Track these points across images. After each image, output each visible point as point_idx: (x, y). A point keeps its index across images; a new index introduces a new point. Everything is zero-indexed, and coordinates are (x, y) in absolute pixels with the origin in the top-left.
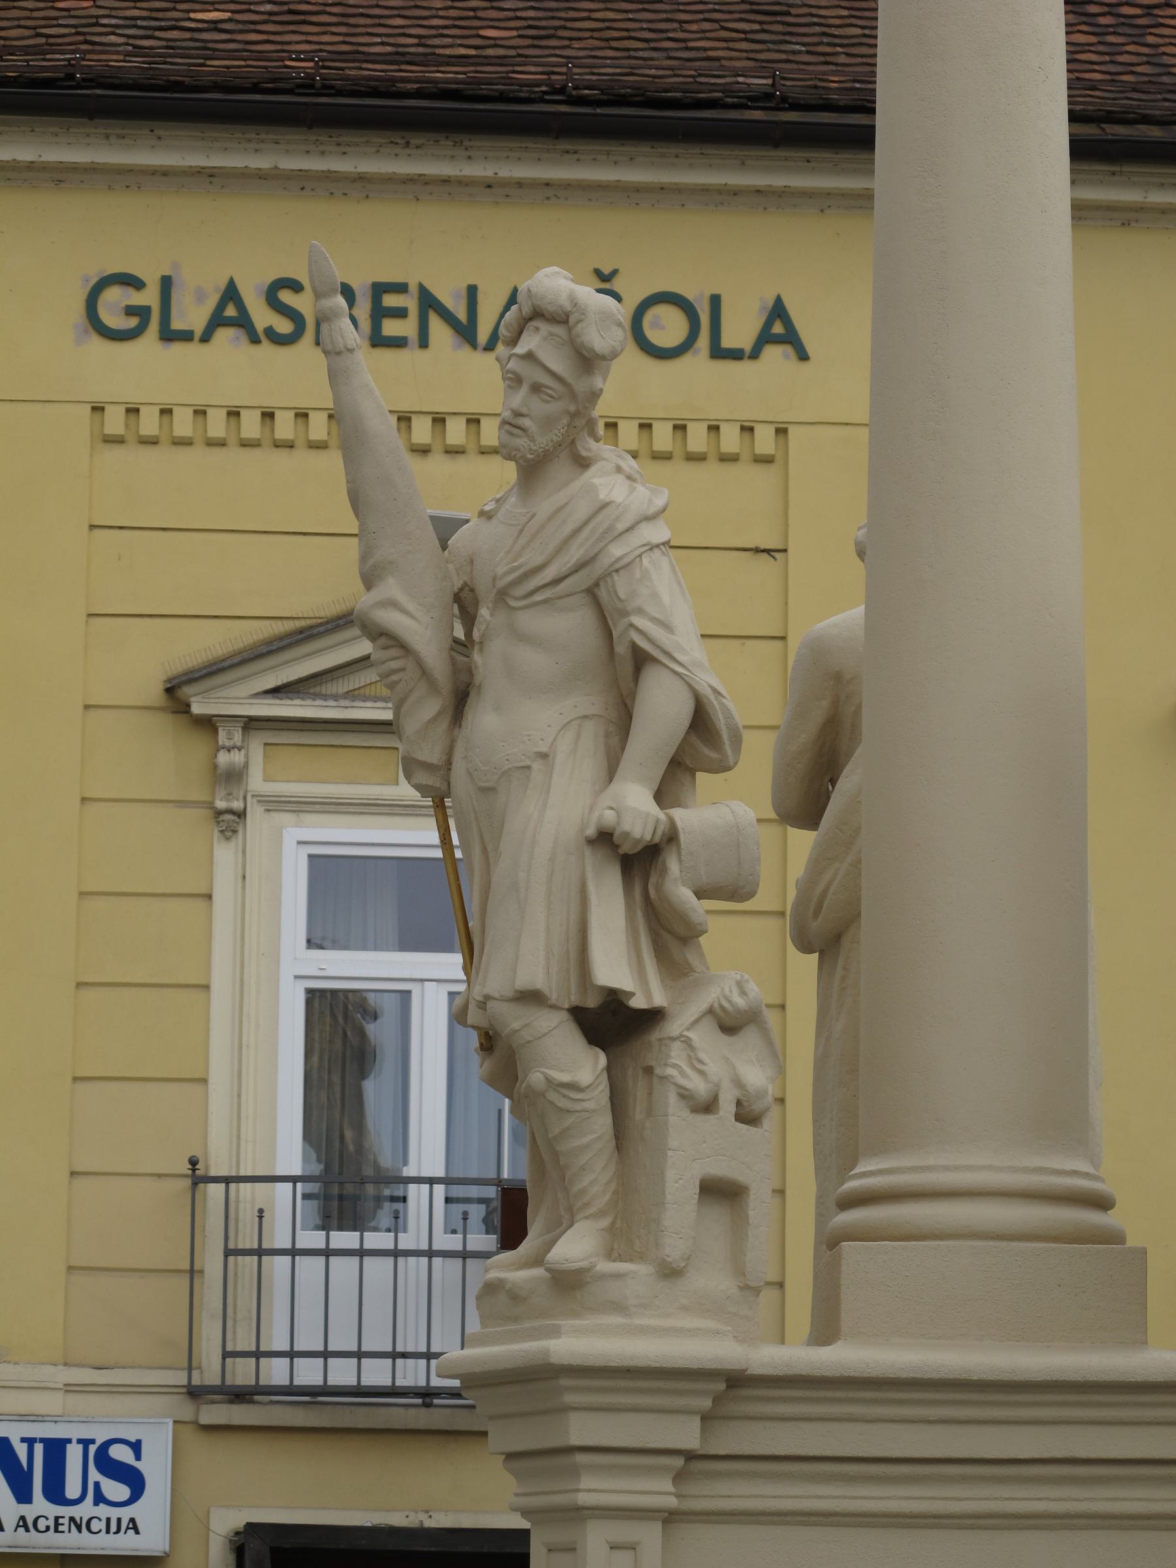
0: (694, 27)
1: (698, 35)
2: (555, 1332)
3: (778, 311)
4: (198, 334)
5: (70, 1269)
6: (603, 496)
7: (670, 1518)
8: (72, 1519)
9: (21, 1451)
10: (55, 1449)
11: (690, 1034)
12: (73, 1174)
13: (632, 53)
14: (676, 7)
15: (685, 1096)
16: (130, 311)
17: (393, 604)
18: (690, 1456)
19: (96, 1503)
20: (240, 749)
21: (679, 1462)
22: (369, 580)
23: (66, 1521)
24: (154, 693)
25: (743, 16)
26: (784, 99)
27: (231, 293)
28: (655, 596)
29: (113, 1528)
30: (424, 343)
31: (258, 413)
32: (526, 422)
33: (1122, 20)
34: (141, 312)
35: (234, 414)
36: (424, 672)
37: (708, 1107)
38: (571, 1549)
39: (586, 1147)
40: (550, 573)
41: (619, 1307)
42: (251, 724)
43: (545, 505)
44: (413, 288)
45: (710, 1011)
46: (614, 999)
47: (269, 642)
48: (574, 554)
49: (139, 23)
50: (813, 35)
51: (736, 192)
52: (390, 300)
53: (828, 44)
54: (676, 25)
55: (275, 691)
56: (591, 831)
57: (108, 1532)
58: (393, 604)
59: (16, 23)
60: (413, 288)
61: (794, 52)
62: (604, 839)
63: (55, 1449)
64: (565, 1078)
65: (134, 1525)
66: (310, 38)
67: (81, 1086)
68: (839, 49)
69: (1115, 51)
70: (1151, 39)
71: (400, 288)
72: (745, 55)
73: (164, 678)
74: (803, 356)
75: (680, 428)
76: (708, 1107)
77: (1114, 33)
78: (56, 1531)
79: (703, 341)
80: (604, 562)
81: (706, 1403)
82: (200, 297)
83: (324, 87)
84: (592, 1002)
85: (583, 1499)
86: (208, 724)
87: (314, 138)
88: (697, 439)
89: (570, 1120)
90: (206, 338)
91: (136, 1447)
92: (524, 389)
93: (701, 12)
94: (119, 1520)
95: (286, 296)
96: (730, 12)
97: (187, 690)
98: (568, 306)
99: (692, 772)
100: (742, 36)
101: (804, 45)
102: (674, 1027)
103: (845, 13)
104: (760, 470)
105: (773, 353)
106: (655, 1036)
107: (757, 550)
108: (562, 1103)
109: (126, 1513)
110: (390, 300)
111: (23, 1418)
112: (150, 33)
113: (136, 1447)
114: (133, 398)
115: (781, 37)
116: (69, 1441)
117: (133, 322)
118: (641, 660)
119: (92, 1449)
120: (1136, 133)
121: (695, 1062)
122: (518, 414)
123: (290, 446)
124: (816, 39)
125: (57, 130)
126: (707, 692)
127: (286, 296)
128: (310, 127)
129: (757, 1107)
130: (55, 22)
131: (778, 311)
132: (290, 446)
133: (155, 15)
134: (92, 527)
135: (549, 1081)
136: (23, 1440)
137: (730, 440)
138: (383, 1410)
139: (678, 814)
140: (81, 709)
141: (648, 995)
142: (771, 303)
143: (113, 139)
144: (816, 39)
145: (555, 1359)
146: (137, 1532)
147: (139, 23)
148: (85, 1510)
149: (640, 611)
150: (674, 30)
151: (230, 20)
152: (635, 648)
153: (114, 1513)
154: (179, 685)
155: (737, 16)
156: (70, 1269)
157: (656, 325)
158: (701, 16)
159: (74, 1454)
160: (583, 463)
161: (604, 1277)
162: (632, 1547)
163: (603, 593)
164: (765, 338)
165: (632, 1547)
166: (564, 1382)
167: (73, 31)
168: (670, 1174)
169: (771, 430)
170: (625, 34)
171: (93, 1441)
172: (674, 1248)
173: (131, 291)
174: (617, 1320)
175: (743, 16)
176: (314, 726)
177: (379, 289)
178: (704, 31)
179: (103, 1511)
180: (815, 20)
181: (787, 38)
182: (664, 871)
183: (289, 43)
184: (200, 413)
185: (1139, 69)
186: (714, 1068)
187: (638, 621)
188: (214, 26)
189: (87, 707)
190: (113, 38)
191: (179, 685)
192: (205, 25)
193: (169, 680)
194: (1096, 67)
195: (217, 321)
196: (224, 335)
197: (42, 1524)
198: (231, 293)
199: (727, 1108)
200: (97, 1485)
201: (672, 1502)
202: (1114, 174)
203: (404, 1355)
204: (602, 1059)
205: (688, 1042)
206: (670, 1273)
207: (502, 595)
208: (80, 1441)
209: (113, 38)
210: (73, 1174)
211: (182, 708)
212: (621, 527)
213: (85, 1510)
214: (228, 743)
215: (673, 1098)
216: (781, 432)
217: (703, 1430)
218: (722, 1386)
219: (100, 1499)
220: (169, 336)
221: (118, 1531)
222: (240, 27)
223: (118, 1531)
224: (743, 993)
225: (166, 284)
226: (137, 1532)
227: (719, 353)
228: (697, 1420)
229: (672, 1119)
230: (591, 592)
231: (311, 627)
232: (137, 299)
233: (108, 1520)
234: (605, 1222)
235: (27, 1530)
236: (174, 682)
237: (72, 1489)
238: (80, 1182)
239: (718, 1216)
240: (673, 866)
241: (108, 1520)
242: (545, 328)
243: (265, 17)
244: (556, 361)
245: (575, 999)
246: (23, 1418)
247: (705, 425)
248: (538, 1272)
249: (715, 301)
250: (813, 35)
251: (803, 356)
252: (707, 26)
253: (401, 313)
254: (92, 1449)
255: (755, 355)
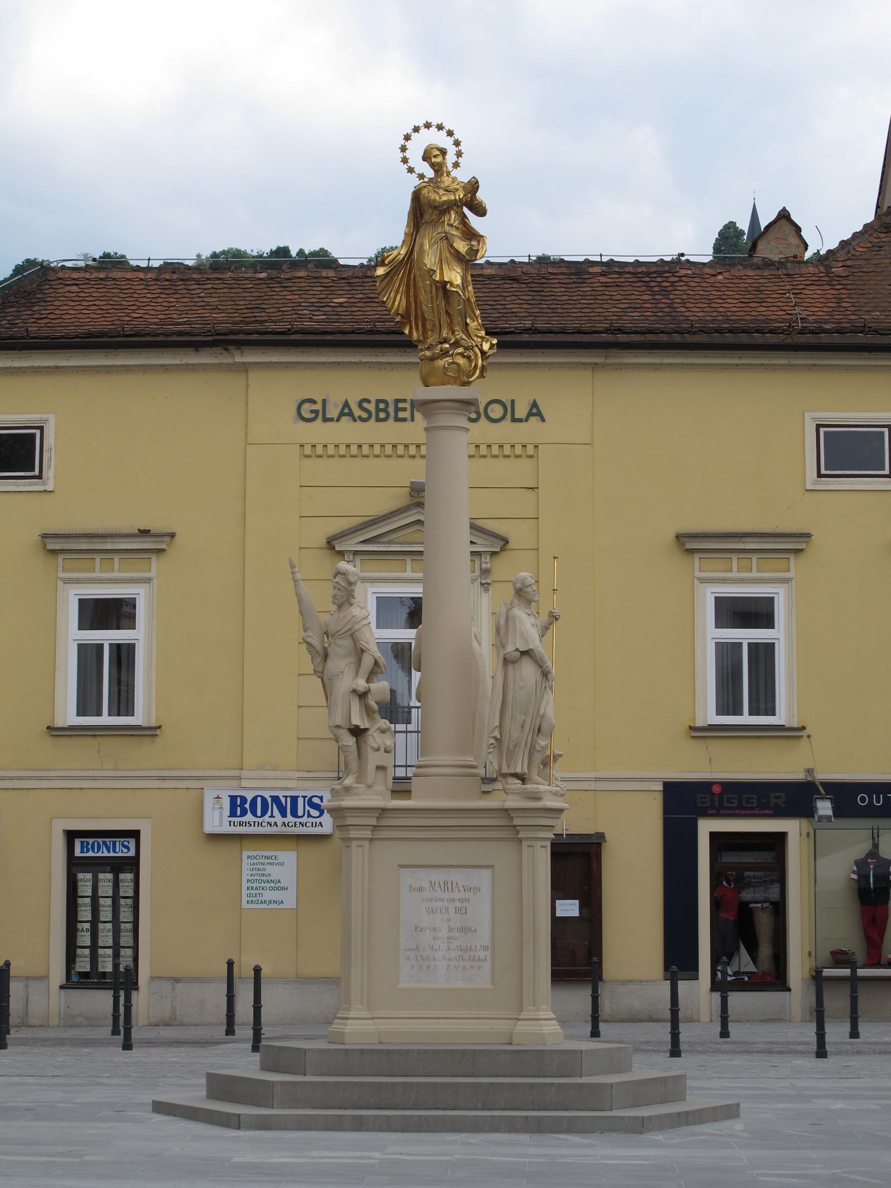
0: (509, 299)
1: (509, 303)
2: (343, 800)
3: (534, 405)
4: (335, 418)
5: (299, 738)
6: (354, 614)
7: (371, 840)
8: (300, 823)
9: (283, 800)
10: (294, 799)
11: (374, 734)
12: (299, 707)
13: (486, 311)
14: (503, 290)
15: (372, 748)
16: (312, 411)
17: (310, 637)
18: (375, 826)
19: (308, 817)
20: (352, 562)
21: (372, 828)
22: (305, 630)
23: (298, 823)
24: (323, 542)
25: (527, 293)
26: (536, 329)
27: (346, 404)
28: (366, 637)
29: (314, 825)
30: (413, 420)
31: (356, 445)
32: (337, 597)
33: (663, 288)
34: (316, 412)
35: (348, 446)
36: (317, 652)
37: (378, 750)
38: (349, 847)
39: (352, 759)
40: (342, 631)
41: (358, 794)
42: (356, 553)
43: (342, 615)
44: (409, 401)
45: (378, 728)
46: (357, 727)
47: (362, 524)
48: (348, 627)
49: (315, 304)
50: (551, 300)
51: (519, 364)
52: (401, 405)
53: (556, 304)
54: (502, 298)
55: (364, 542)
56: (351, 690)
57: (312, 826)
58: (310, 637)
59: (272, 306)
60: (409, 401)
61: (543, 308)
62: (354, 691)
63: (294, 799)
64: (346, 744)
65: (321, 824)
66: (374, 309)
67: (301, 677)
68: (559, 306)
69: (658, 302)
70: (672, 297)
71: (404, 401)
72: (525, 310)
73: (326, 537)
74: (543, 420)
75: (501, 446)
76: (378, 750)
77: (659, 294)
78: (295, 826)
79: (509, 416)
80: (354, 629)
81: (377, 815)
82: (336, 406)
83: (377, 331)
84: (352, 727)
85: (351, 836)
86: (341, 554)
87: (373, 350)
88: (507, 450)
89: (348, 753)
90: (338, 420)
91: (321, 798)
92: (337, 590)
93: (512, 292)
94: (316, 823)
95: (365, 405)
96: (522, 292)
97: (333, 542)
98: (345, 571)
99: (376, 674)
100: (525, 302)
101: (547, 305)
102: (370, 732)
103: (563, 290)
104: (528, 461)
105: (533, 419)
106: (367, 734)
107: (528, 488)
108: (346, 750)
109: (318, 820)
110: (401, 405)
111: (283, 789)
112: (318, 309)
113: (321, 798)
114: (314, 442)
115: (539, 302)
116: (299, 796)
117: (313, 415)
118: (363, 651)
119: (307, 799)
120: (658, 339)
121: (374, 740)
122: (335, 595)
123: (367, 456)
124: (551, 302)
125: (285, 350)
126: (377, 657)
127: (365, 405)
128: (371, 348)
129: (390, 749)
130: (285, 305)
131: (534, 405)
132: (367, 456)
133: (320, 301)
134: (301, 486)
135: (343, 745)
136: (284, 796)
137: (518, 450)
138: (404, 784)
139: (371, 685)
140: (298, 549)
141: (365, 725)
142: (532, 402)
143: (304, 353)
144: (551, 302)
145: (343, 806)
146: (322, 826)
147: (315, 304)
148: (305, 819)
149: (362, 640)
150: (502, 300)
151: (347, 302)
152: (361, 648)
153: (314, 820)
154: (331, 541)
155: (524, 293)
156: (299, 738)
157: (492, 411)
158: (512, 294)
159: (300, 801)
160: (351, 605)
161: (355, 788)
162: (362, 846)
163: (354, 635)
164: (530, 414)
165: (362, 846)
166: (346, 811)
167: (292, 309)
168: (369, 765)
169: (532, 446)
170: (484, 303)
171: (307, 797)
172: (370, 781)
173: (312, 404)
174: (357, 797)
175: (527, 293)
176: (377, 553)
177: (397, 401)
178: (512, 300)
179: (311, 819)
180: (552, 293)
181: (541, 302)
182: (368, 698)
183: (366, 311)
184: (337, 446)
185: (664, 310)
186: (379, 741)
187: (362, 643)
188: (341, 305)
189: (300, 548)
190: (305, 312)
191: (331, 541)
192: (338, 305)
193: (328, 539)
194: (650, 310)
195: (342, 414)
196: (344, 419)
197: (290, 824)
198: (346, 404)
199: (382, 750)
200: (308, 811)
201: (371, 836)
202: (650, 353)
203: (409, 766)
204: (355, 739)
205: (373, 736)
206: (369, 787)
207: (333, 635)
208: (302, 797)
209: (305, 312)
210: (299, 707)
211: (333, 548)
212: (358, 621)
213: (305, 819)
214: (348, 560)
215: (369, 749)
216: (536, 447)
217: (377, 821)
218: (380, 811)
219: (309, 816)
220: (326, 420)
221: (316, 826)
222: (350, 305)
223: (316, 826)
224: (385, 724)
225: (324, 401)
226: (322, 826)
227: (514, 420)
228: (375, 818)
229: (369, 753)
230: (352, 635)
231: (376, 519)
232: (315, 407)
233: (312, 823)
234: (356, 775)
235: (285, 826)
236: (330, 540)
237: (300, 813)
238: (302, 709)
239: (381, 774)
240: (370, 696)
241: (312, 823)
242: (341, 576)
243: (359, 300)
244: (343, 584)
245: (348, 726)
246: (283, 789)
247: (509, 445)
248: (340, 786)
249: (513, 402)
250: (551, 300)
251: (543, 420)
252: (513, 298)
253: (405, 409)
254: (307, 799)
255: (527, 420)
